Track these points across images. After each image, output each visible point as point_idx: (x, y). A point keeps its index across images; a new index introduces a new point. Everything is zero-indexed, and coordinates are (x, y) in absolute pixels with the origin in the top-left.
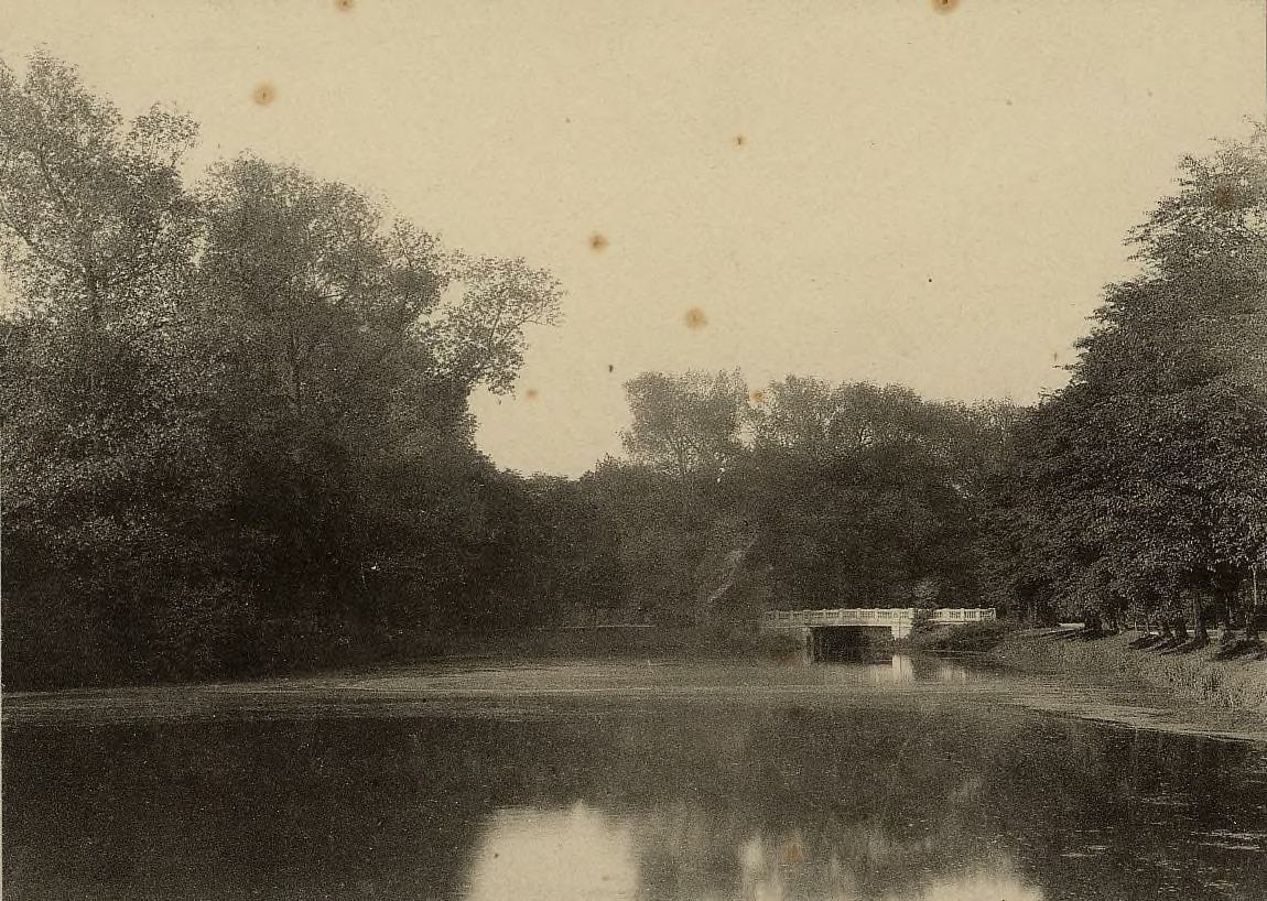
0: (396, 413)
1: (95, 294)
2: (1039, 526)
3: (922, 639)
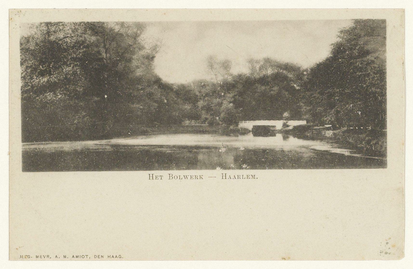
0: (135, 63)
1: (48, 28)
2: (319, 97)
3: (284, 129)
